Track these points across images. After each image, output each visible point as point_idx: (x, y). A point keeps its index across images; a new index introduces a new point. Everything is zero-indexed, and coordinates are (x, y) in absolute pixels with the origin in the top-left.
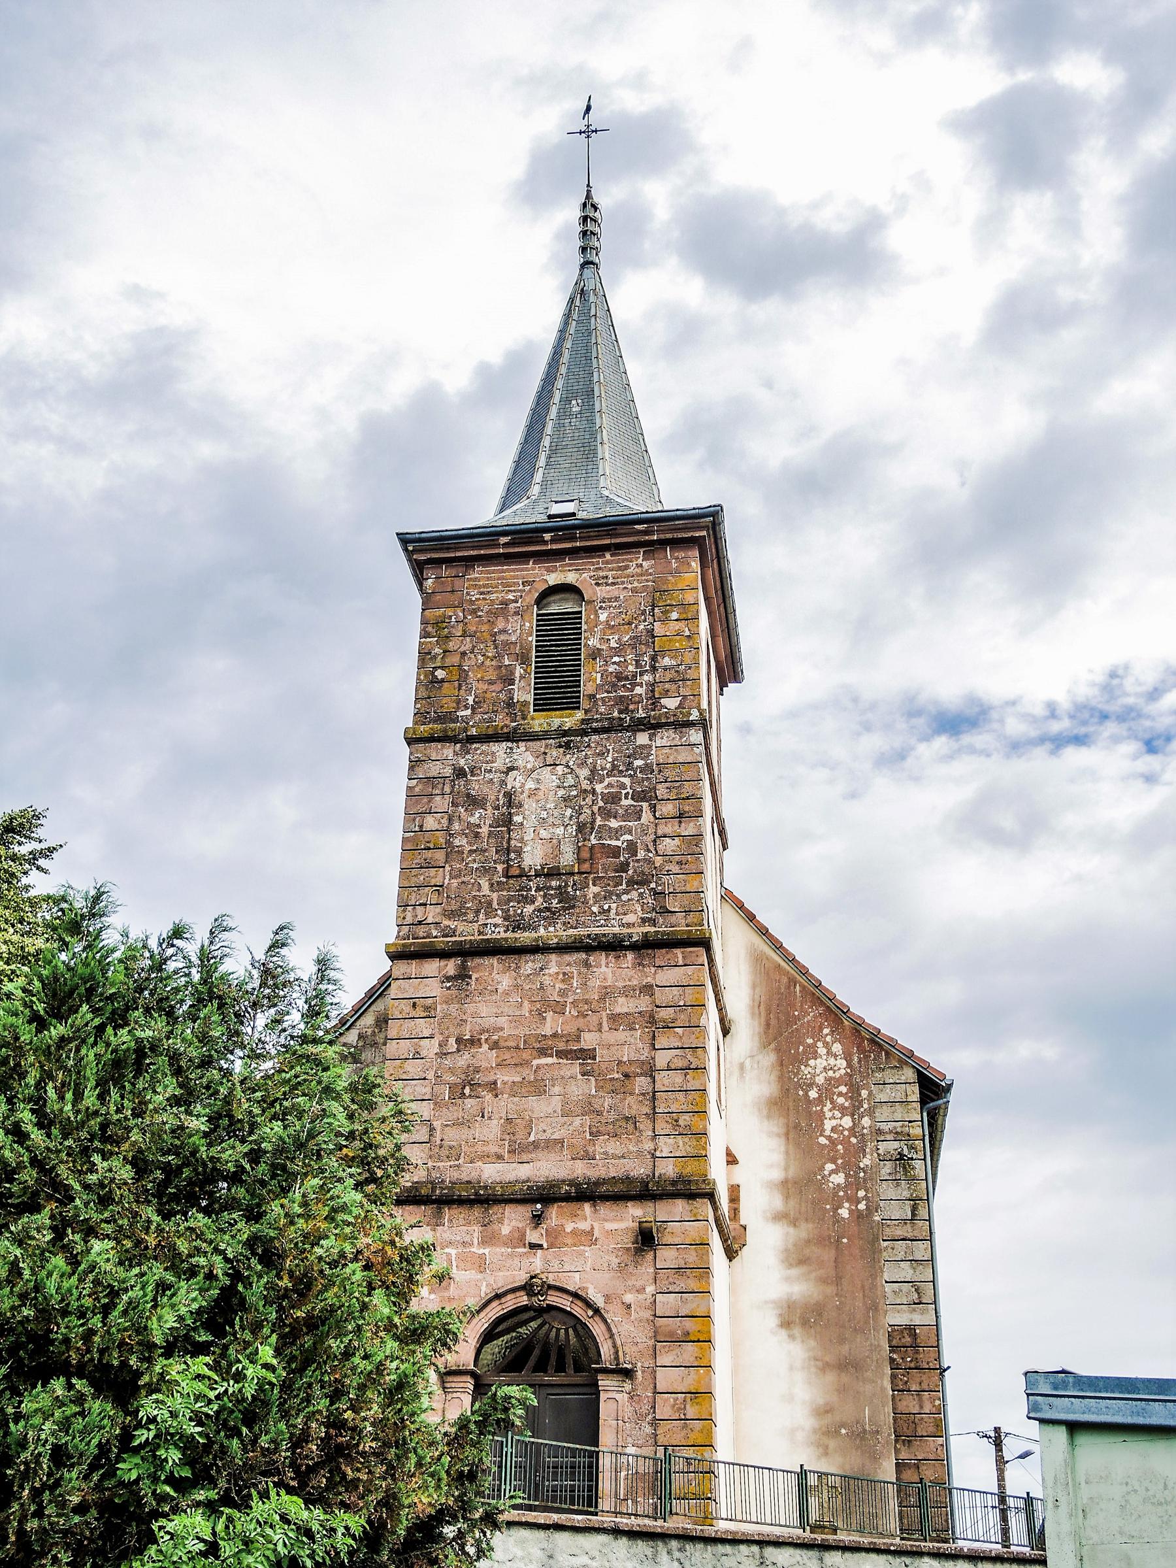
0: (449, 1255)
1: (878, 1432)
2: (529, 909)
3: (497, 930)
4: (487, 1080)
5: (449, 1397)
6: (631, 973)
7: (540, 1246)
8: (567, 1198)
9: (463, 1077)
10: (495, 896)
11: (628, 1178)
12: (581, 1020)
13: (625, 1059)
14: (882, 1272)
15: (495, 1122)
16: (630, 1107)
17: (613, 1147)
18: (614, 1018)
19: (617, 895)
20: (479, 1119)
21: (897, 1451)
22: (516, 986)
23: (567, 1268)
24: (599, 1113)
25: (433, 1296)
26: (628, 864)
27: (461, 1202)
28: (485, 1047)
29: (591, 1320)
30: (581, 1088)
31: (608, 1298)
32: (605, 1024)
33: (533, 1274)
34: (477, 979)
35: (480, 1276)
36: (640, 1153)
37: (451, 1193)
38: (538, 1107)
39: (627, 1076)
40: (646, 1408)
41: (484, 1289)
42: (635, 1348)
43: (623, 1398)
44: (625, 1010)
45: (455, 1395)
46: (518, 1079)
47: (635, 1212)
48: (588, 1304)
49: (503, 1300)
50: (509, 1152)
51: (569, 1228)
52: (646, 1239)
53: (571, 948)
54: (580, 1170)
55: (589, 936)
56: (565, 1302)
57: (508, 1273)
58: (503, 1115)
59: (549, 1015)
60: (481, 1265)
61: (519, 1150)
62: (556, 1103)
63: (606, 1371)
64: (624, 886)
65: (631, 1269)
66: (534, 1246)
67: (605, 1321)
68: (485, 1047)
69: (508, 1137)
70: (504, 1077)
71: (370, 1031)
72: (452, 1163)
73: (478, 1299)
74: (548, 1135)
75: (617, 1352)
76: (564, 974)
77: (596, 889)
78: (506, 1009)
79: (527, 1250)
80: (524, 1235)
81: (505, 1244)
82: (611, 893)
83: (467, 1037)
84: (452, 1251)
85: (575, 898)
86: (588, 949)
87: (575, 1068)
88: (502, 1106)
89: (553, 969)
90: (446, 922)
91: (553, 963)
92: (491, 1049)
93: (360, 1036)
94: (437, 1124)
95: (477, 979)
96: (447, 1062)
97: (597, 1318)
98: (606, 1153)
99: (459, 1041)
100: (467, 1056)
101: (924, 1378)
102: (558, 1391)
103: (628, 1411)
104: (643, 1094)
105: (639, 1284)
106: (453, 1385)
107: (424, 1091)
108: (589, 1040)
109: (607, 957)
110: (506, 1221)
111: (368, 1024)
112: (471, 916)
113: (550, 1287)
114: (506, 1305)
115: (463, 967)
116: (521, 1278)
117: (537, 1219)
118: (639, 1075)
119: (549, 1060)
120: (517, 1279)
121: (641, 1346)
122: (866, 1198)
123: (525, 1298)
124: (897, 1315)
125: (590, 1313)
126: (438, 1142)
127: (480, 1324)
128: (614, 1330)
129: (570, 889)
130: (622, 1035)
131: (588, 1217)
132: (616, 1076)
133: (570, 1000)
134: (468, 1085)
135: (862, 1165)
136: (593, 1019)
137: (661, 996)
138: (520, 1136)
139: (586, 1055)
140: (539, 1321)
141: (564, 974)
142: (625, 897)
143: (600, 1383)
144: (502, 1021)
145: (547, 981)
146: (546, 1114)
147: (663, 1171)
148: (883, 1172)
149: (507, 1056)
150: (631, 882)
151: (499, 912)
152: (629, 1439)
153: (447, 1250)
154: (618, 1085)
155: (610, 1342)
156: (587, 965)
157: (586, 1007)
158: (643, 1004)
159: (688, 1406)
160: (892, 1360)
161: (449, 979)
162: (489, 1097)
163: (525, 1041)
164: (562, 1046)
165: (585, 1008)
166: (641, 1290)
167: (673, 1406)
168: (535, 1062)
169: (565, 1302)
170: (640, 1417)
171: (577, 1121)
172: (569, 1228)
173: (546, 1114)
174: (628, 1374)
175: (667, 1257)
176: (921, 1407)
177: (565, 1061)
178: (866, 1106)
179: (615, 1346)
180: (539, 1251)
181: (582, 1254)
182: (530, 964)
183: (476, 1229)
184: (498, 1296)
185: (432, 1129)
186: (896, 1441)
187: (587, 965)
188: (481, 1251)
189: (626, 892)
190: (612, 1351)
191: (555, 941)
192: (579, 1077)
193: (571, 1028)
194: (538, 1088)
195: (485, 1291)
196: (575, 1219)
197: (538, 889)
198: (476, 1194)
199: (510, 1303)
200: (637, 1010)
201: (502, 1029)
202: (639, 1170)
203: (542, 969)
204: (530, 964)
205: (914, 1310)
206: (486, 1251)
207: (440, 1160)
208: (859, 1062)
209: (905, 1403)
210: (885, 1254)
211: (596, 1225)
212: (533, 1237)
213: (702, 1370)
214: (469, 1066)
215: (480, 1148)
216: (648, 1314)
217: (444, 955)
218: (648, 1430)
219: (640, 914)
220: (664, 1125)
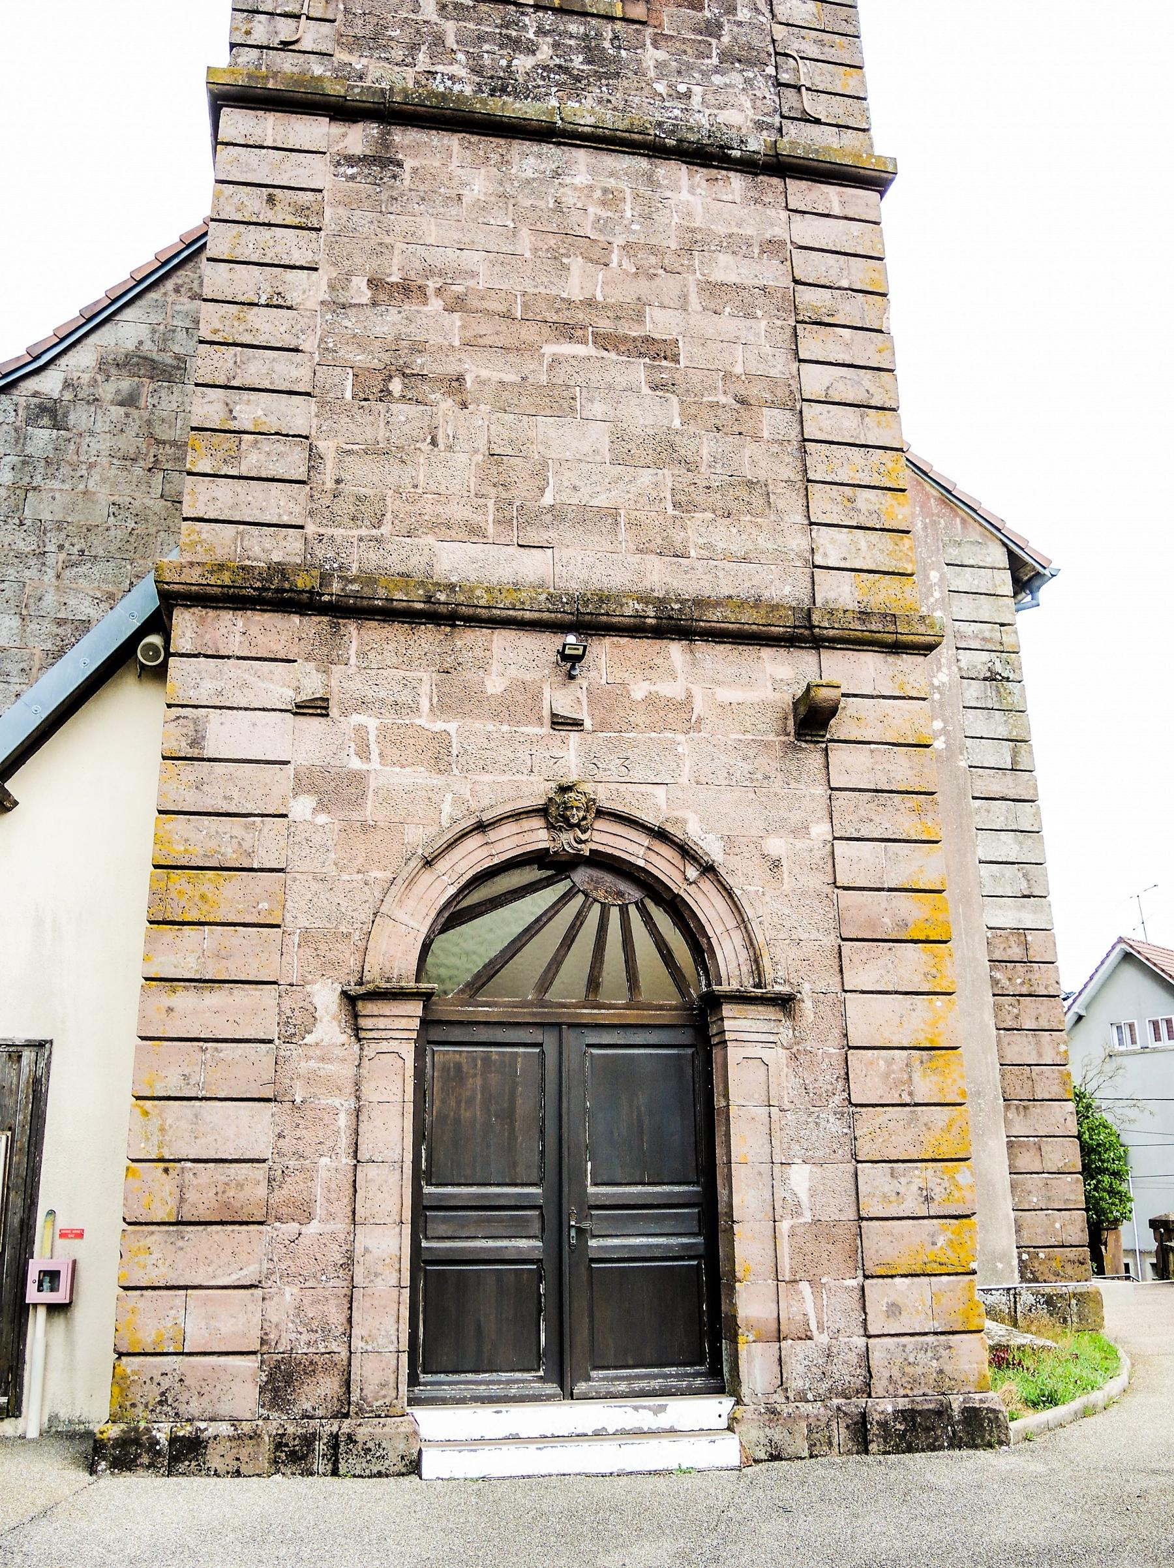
0: (360, 729)
1: (979, 1093)
2: (523, 63)
3: (456, 79)
4: (440, 370)
5: (371, 1050)
6: (740, 212)
7: (577, 724)
8: (635, 630)
9: (386, 357)
10: (450, 27)
11: (758, 600)
12: (643, 282)
13: (738, 369)
14: (975, 846)
15: (461, 458)
16: (754, 464)
17: (724, 537)
18: (712, 289)
19: (702, 72)
20: (425, 446)
21: (1007, 1122)
22: (503, 195)
23: (636, 775)
24: (690, 466)
25: (322, 819)
26: (720, 26)
27: (389, 614)
28: (436, 304)
29: (692, 889)
30: (651, 414)
31: (729, 841)
32: (693, 298)
33: (565, 781)
34: (415, 170)
35: (437, 780)
36: (780, 555)
37: (367, 592)
38: (552, 436)
39: (743, 402)
40: (827, 1078)
41: (447, 808)
42: (794, 952)
43: (777, 1057)
44: (732, 278)
45: (384, 1047)
46: (512, 377)
47: (781, 675)
48: (686, 852)
49: (493, 835)
50: (497, 522)
51: (639, 691)
52: (812, 720)
53: (623, 142)
54: (660, 578)
55: (660, 124)
56: (633, 848)
57: (505, 778)
58: (482, 445)
59: (576, 264)
60: (440, 755)
61: (521, 521)
62: (598, 436)
63: (741, 998)
64: (715, 60)
65: (777, 786)
66: (559, 722)
67: (728, 892)
68: (436, 304)
69: (492, 491)
70: (479, 370)
71: (86, 378)
72: (363, 532)
73: (433, 830)
74: (583, 496)
75: (756, 960)
76: (605, 191)
77: (661, 55)
78: (480, 238)
79: (546, 730)
80: (537, 697)
81: (495, 716)
82: (690, 67)
83: (394, 279)
84: (371, 723)
85: (617, 60)
86: (656, 150)
87: (639, 371)
88: (480, 425)
89: (582, 178)
90: (342, 56)
91: (582, 167)
92: (450, 310)
93: (67, 385)
94: (326, 446)
95: (415, 170)
96: (350, 322)
97: (707, 885)
98: (708, 546)
99: (374, 283)
100: (393, 316)
101: (1042, 1009)
102: (606, 1038)
103: (786, 1085)
104: (781, 443)
105: (795, 817)
106: (381, 1023)
107: (295, 373)
108: (660, 323)
109: (690, 177)
110: (495, 667)
111: (83, 365)
112: (398, 54)
113: (600, 813)
114: (499, 847)
115: (384, 142)
116: (537, 791)
117: (570, 661)
118: (772, 405)
119: (580, 350)
120: (526, 791)
121: (808, 949)
122: (944, 731)
123: (543, 834)
124: (999, 912)
125: (692, 873)
126: (330, 485)
127: (439, 886)
128: (750, 912)
129: (607, 44)
130: (728, 324)
131: (677, 666)
132: (723, 400)
133: (619, 241)
134: (393, 377)
135: (936, 683)
136: (669, 286)
137: (810, 266)
138: (522, 491)
139: (657, 351)
140: (562, 887)
141: (605, 191)
142: (717, 79)
143: (727, 1024)
144: (472, 259)
145: (570, 198)
146: (574, 452)
147: (832, 595)
148: (967, 694)
149: (486, 327)
150: (726, 56)
151: (461, 56)
152: (796, 1147)
153: (356, 719)
154: (725, 417)
155: (738, 937)
156: (650, 179)
157: (653, 260)
158: (772, 274)
159: (916, 1077)
160: (995, 982)
161: (351, 160)
162: (447, 405)
163: (525, 305)
164: (605, 325)
165: (650, 260)
166: (801, 830)
167: (887, 1075)
168: (549, 349)
169: (633, 848)
170: (814, 1099)
171: (646, 477)
172: (639, 691)
173: (574, 452)
174: (785, 1003)
175: (849, 765)
176: (1040, 1055)
177: (613, 355)
178: (937, 595)
179: (750, 943)
180: (574, 737)
181: (668, 748)
182: (531, 160)
183: (426, 679)
184: (481, 827)
185: (314, 457)
186: (1007, 1108)
187: (650, 179)
188: (439, 726)
189: (717, 70)
190: (743, 955)
191: (591, 120)
192: (645, 390)
193: (625, 293)
194: (559, 401)
195: (450, 813)
196: (653, 675)
197: (540, 31)
198: (428, 600)
199: (507, 844)
200: (757, 283)
201: (473, 274)
202: (784, 588)
203: (556, 174)
204: (531, 160)
205: (1023, 906)
206: (452, 727)
207: (333, 520)
208: (925, 528)
209: (1016, 1048)
210: (977, 819)
211: (697, 691)
212: (564, 700)
213: (939, 1001)
214: (398, 338)
215: (429, 508)
216: (818, 881)
217: (342, 111)
218: (836, 1126)
219: (750, 112)
220: (828, 507)
